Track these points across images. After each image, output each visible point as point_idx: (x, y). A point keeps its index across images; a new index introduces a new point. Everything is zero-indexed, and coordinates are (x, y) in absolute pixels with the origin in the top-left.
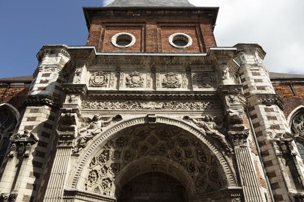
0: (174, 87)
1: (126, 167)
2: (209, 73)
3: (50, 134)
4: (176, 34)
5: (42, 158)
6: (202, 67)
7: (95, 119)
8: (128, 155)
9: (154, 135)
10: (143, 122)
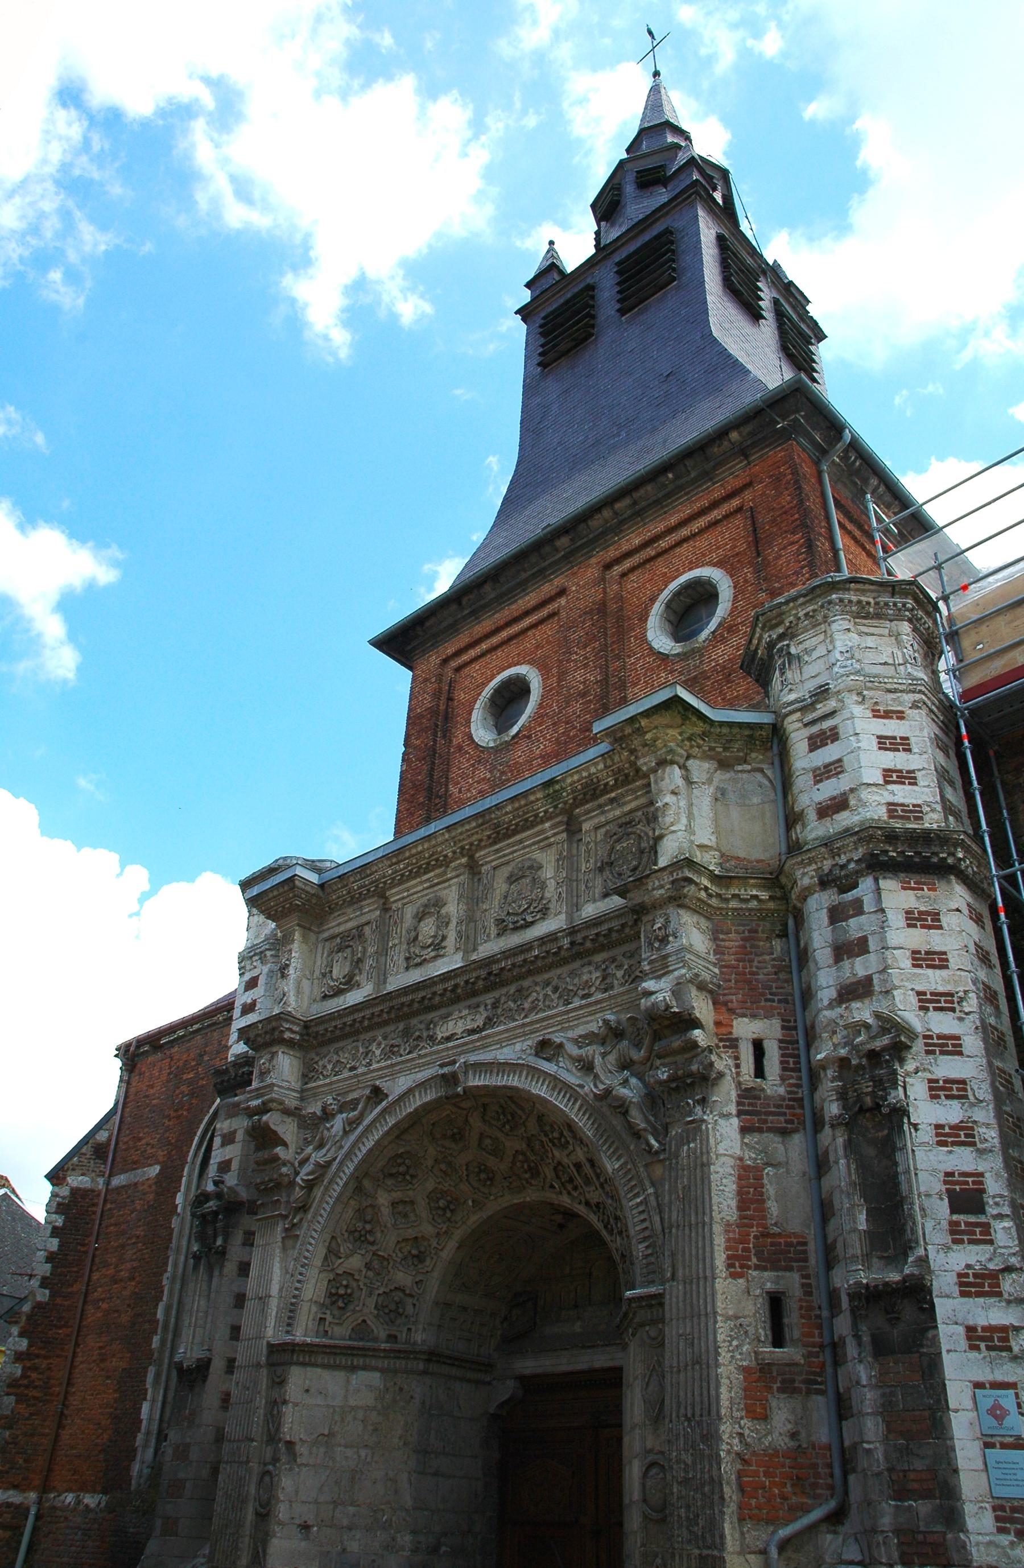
1: (452, 1244)
4: (666, 592)
6: (612, 801)
7: (327, 1115)
10: (429, 1096)
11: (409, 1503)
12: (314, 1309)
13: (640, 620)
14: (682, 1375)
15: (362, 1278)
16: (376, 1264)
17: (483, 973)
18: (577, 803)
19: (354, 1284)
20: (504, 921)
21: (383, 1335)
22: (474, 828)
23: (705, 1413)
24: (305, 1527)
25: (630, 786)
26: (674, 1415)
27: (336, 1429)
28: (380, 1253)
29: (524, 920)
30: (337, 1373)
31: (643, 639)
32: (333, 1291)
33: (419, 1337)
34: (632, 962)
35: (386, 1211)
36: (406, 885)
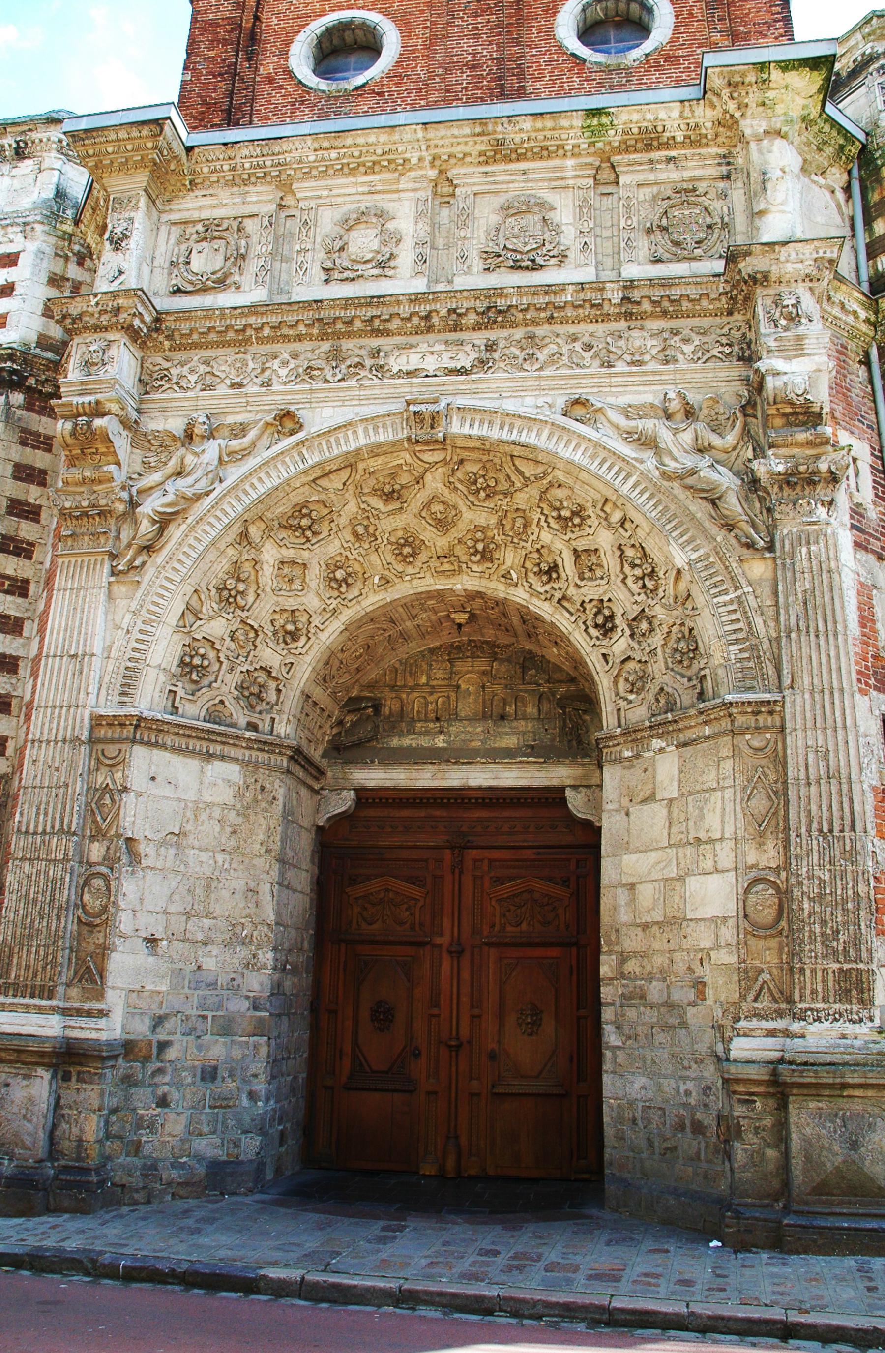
0: (535, 267)
1: (336, 626)
2: (702, 187)
3: (40, 507)
5: (20, 600)
6: (670, 160)
8: (340, 574)
9: (440, 486)
11: (271, 918)
12: (162, 678)
13: (546, 11)
14: (813, 789)
15: (224, 649)
16: (240, 635)
17: (481, 306)
18: (626, 148)
19: (212, 655)
20: (500, 256)
21: (242, 721)
22: (467, 136)
23: (847, 828)
24: (152, 941)
25: (698, 151)
26: (803, 830)
27: (189, 827)
28: (249, 621)
29: (533, 261)
30: (188, 760)
31: (549, 33)
32: (188, 659)
33: (282, 729)
34: (705, 339)
35: (268, 572)
36: (329, 182)
